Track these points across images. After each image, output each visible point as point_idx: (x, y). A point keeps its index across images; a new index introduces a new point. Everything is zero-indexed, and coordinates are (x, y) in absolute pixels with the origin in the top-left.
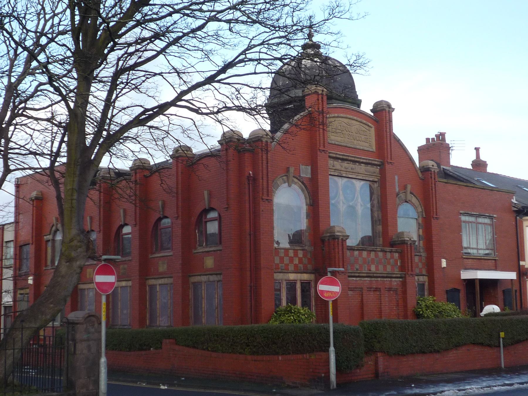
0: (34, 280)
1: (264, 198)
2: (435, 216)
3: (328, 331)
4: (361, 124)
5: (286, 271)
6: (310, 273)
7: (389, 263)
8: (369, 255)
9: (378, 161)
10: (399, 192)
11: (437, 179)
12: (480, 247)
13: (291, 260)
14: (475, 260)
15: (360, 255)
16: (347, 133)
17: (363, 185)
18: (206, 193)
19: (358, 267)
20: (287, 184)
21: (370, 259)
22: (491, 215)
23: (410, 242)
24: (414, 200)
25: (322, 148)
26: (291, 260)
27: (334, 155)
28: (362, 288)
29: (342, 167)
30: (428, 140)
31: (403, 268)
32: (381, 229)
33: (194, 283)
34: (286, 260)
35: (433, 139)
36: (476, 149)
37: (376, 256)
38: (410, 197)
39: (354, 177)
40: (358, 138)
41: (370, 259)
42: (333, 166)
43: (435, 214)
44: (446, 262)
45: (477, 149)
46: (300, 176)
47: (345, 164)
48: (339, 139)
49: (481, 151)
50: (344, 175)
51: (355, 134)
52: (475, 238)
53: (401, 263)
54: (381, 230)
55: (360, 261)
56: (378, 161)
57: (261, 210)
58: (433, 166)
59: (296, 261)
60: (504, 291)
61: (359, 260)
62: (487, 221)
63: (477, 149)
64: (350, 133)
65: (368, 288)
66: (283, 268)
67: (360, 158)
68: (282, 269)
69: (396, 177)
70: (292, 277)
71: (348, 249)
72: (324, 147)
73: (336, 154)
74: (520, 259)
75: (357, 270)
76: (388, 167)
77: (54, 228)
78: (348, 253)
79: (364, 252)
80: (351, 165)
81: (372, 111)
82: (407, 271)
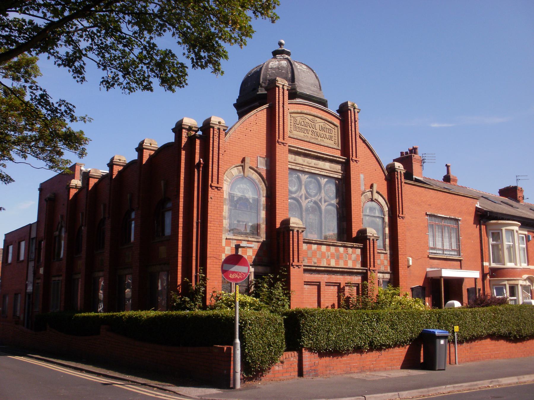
0: (45, 271)
1: (213, 185)
7: (350, 259)
9: (343, 159)
16: (310, 129)
17: (327, 182)
18: (162, 183)
19: (316, 261)
22: (457, 218)
23: (373, 238)
24: (380, 199)
25: (281, 140)
29: (304, 161)
30: (402, 153)
32: (345, 225)
35: (407, 153)
36: (446, 165)
37: (337, 251)
38: (376, 196)
40: (322, 135)
43: (401, 213)
45: (448, 167)
46: (257, 167)
49: (450, 168)
52: (440, 239)
54: (345, 227)
56: (343, 159)
57: (209, 197)
60: (468, 289)
64: (314, 130)
69: (362, 176)
71: (304, 242)
72: (284, 139)
74: (484, 260)
75: (315, 263)
76: (352, 164)
77: (60, 226)
78: (305, 247)
82: (369, 266)
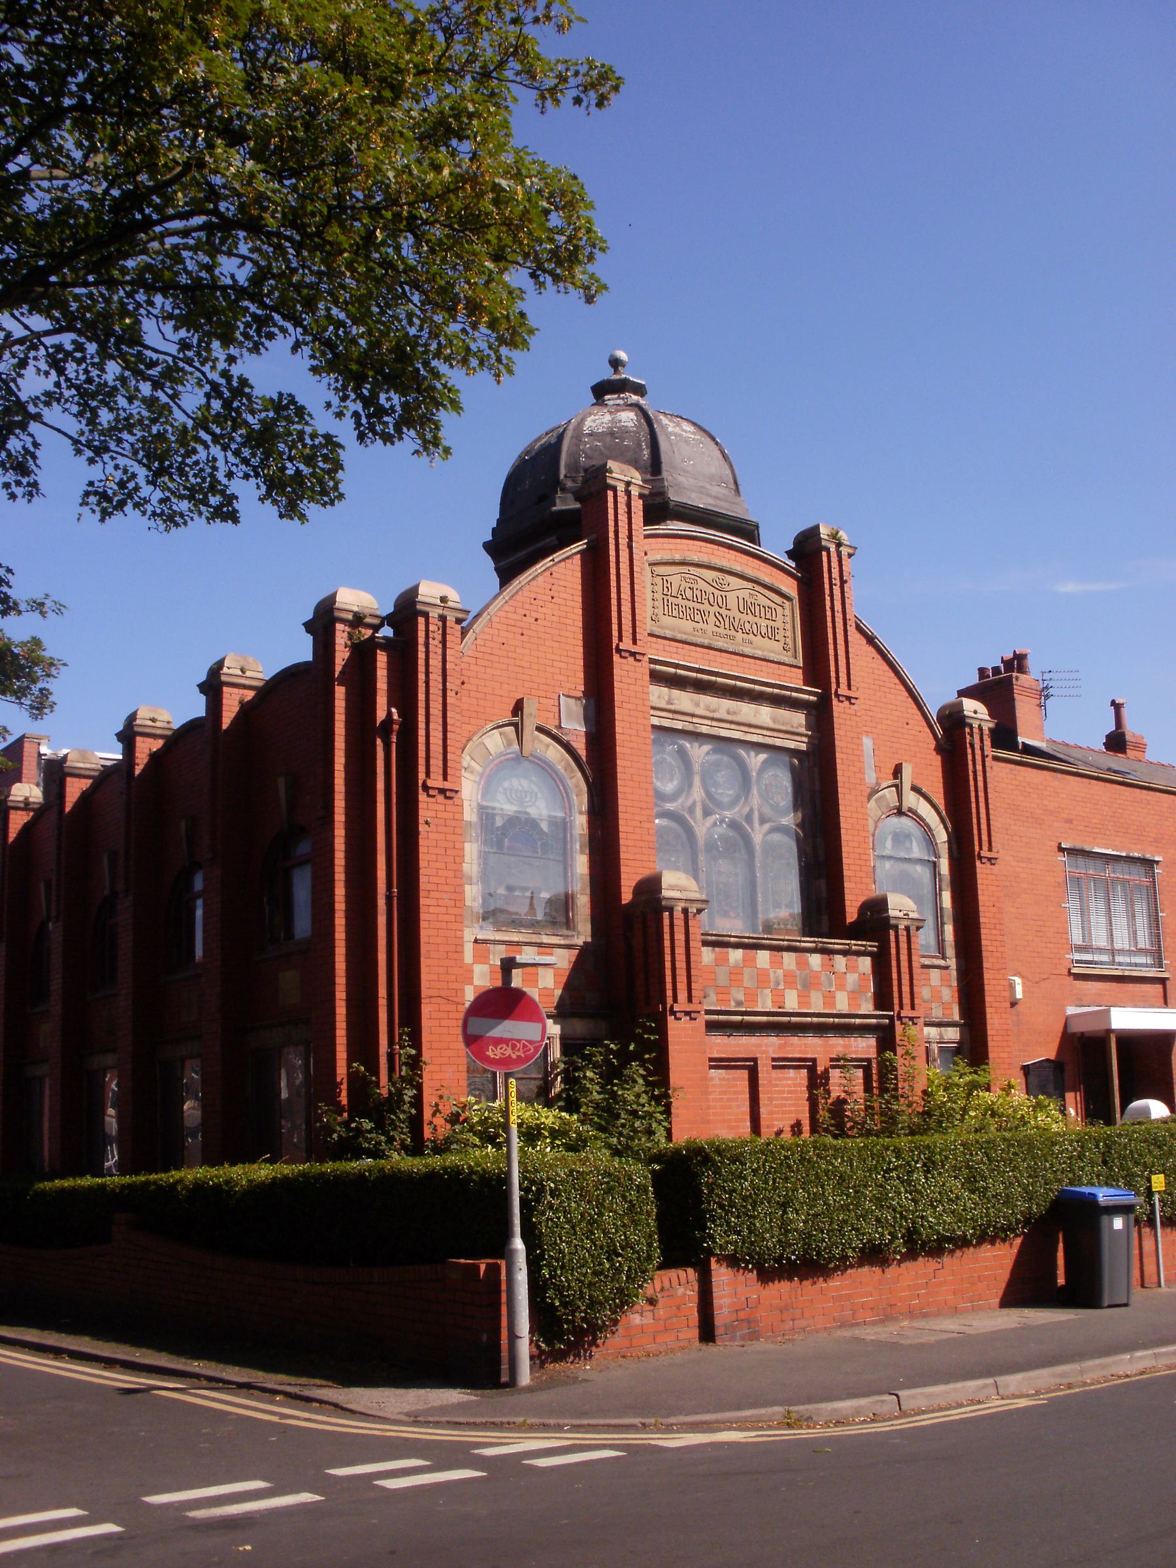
1: (430, 783)
2: (985, 853)
3: (506, 1196)
4: (758, 588)
6: (1064, 1100)
7: (841, 987)
9: (810, 693)
10: (878, 784)
11: (988, 750)
12: (1117, 946)
15: (749, 962)
17: (765, 762)
18: (281, 783)
22: (1148, 856)
23: (906, 923)
24: (925, 809)
25: (626, 644)
28: (755, 1060)
30: (982, 671)
31: (883, 998)
35: (996, 670)
36: (1113, 703)
38: (911, 799)
44: (1023, 984)
45: (1117, 707)
46: (559, 727)
47: (707, 701)
49: (1125, 712)
51: (738, 615)
52: (1103, 920)
54: (824, 895)
56: (810, 693)
57: (421, 820)
58: (975, 712)
61: (746, 977)
63: (1117, 707)
65: (774, 1060)
71: (705, 943)
75: (739, 1003)
78: (707, 956)
81: (791, 554)
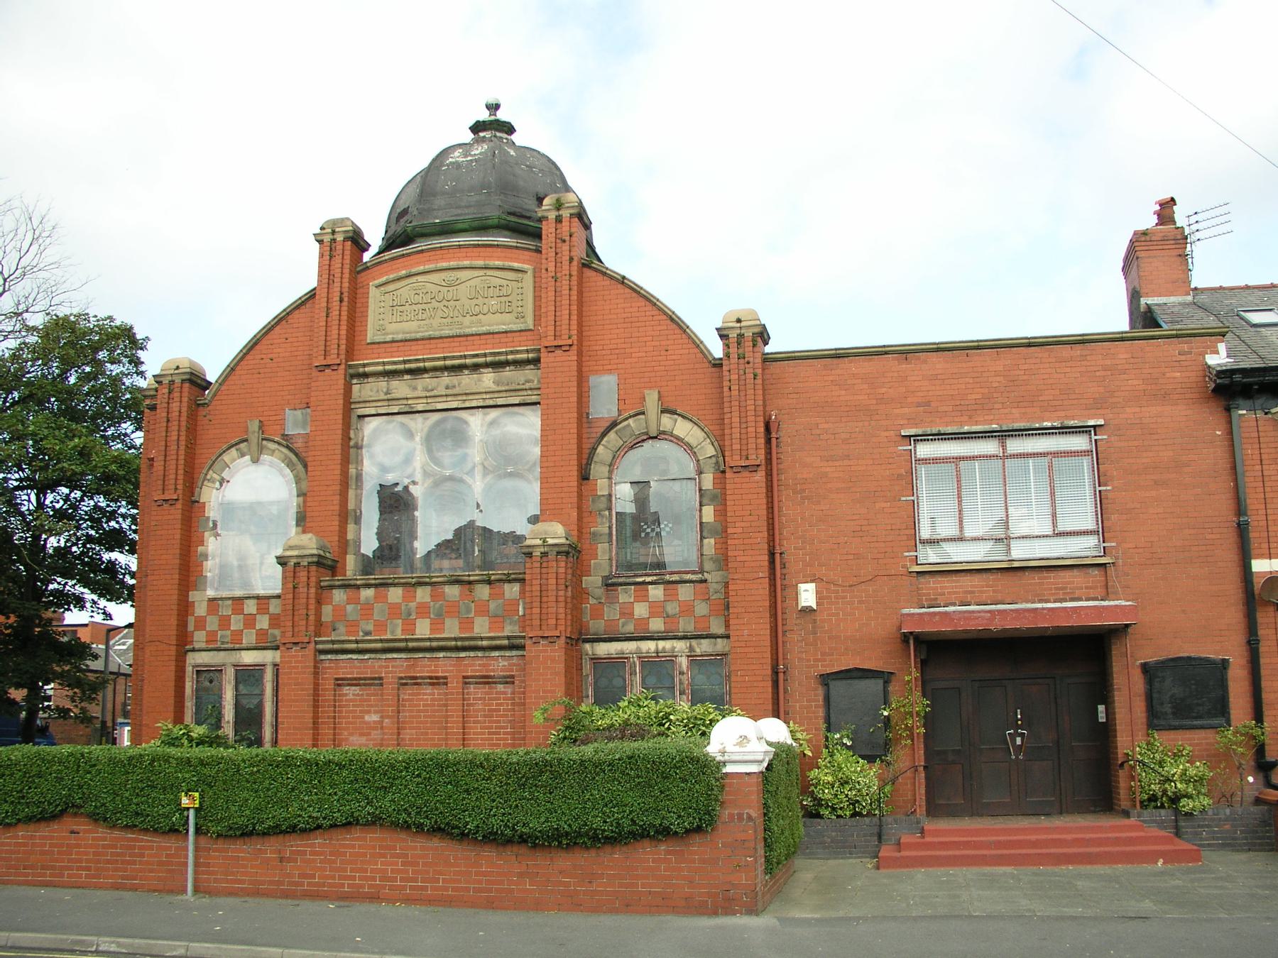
5: (237, 646)
8: (408, 598)
13: (250, 621)
14: (991, 577)
20: (248, 458)
21: (413, 605)
26: (250, 621)
27: (380, 368)
28: (381, 678)
33: (596, 660)
34: (236, 623)
39: (454, 405)
41: (413, 605)
42: (386, 393)
48: (413, 325)
50: (420, 408)
53: (186, 626)
55: (379, 612)
59: (263, 622)
62: (1079, 442)
66: (228, 639)
67: (465, 357)
68: (223, 643)
70: (249, 658)
73: (384, 364)
75: (367, 633)
79: (392, 589)
80: (446, 379)
